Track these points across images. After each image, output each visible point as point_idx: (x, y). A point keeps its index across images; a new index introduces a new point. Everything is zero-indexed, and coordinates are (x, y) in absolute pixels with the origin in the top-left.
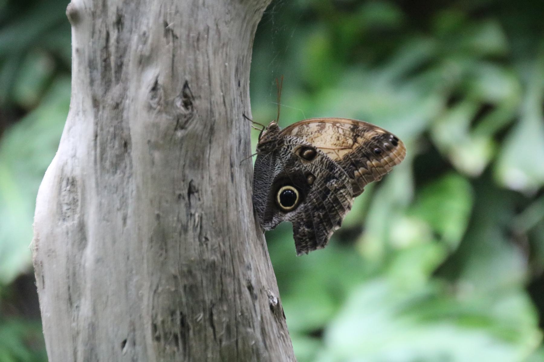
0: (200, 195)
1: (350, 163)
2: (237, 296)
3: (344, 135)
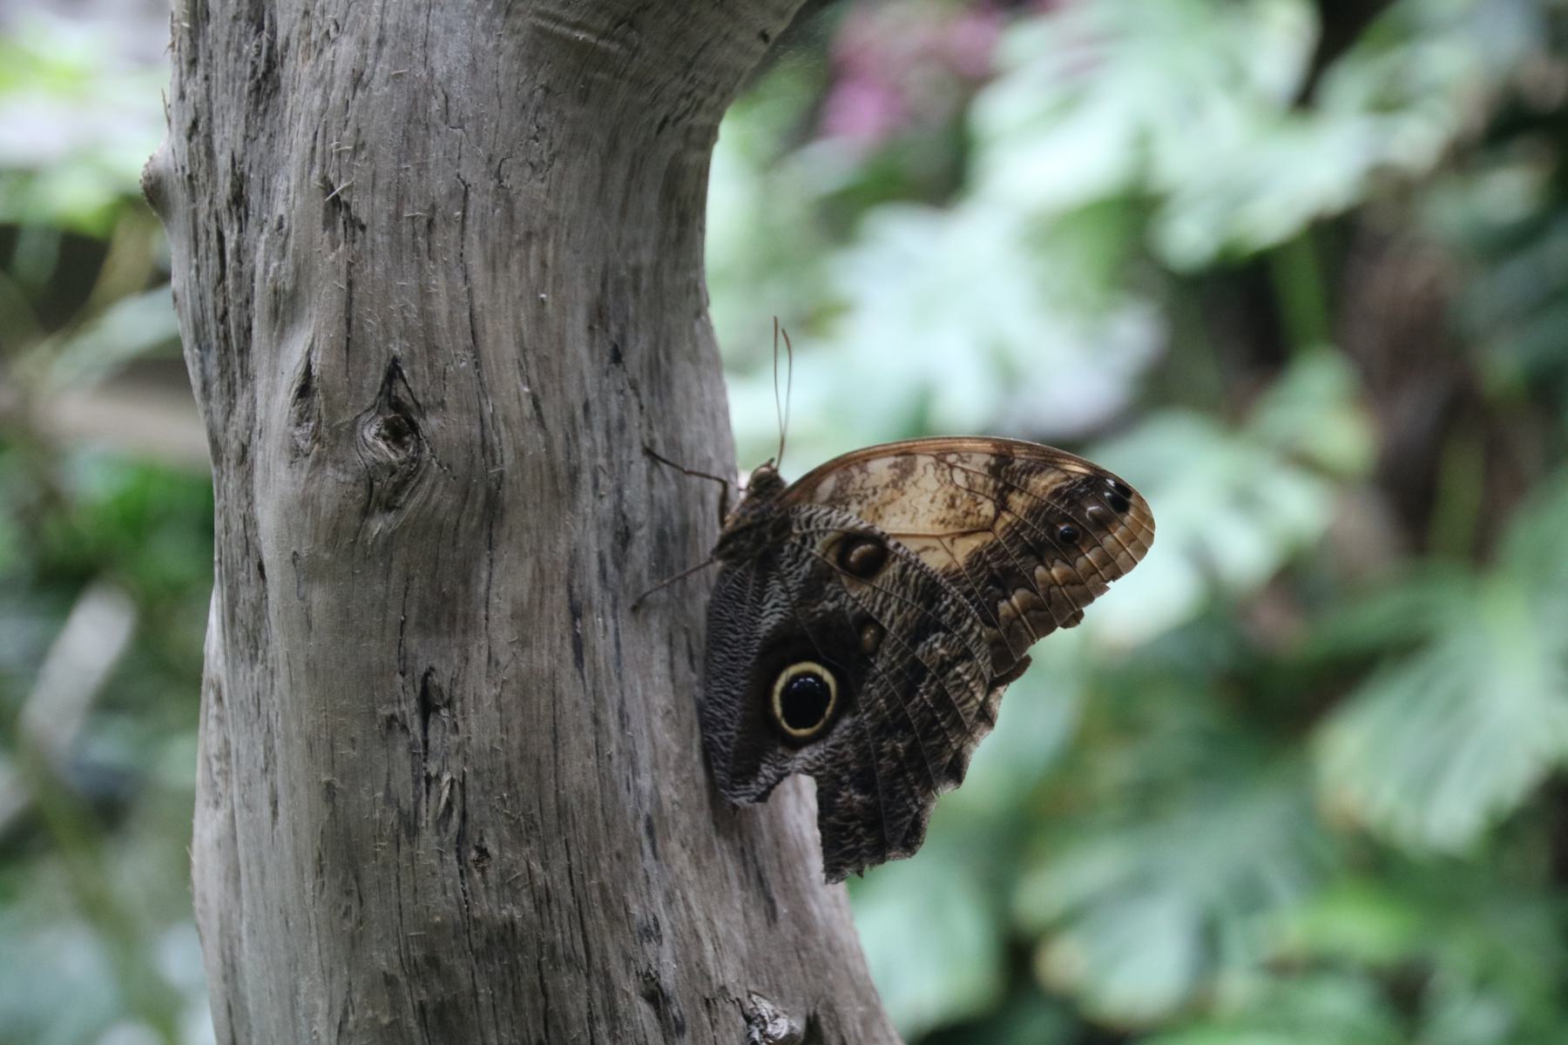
0: (458, 712)
1: (986, 578)
2: (602, 1028)
3: (969, 490)
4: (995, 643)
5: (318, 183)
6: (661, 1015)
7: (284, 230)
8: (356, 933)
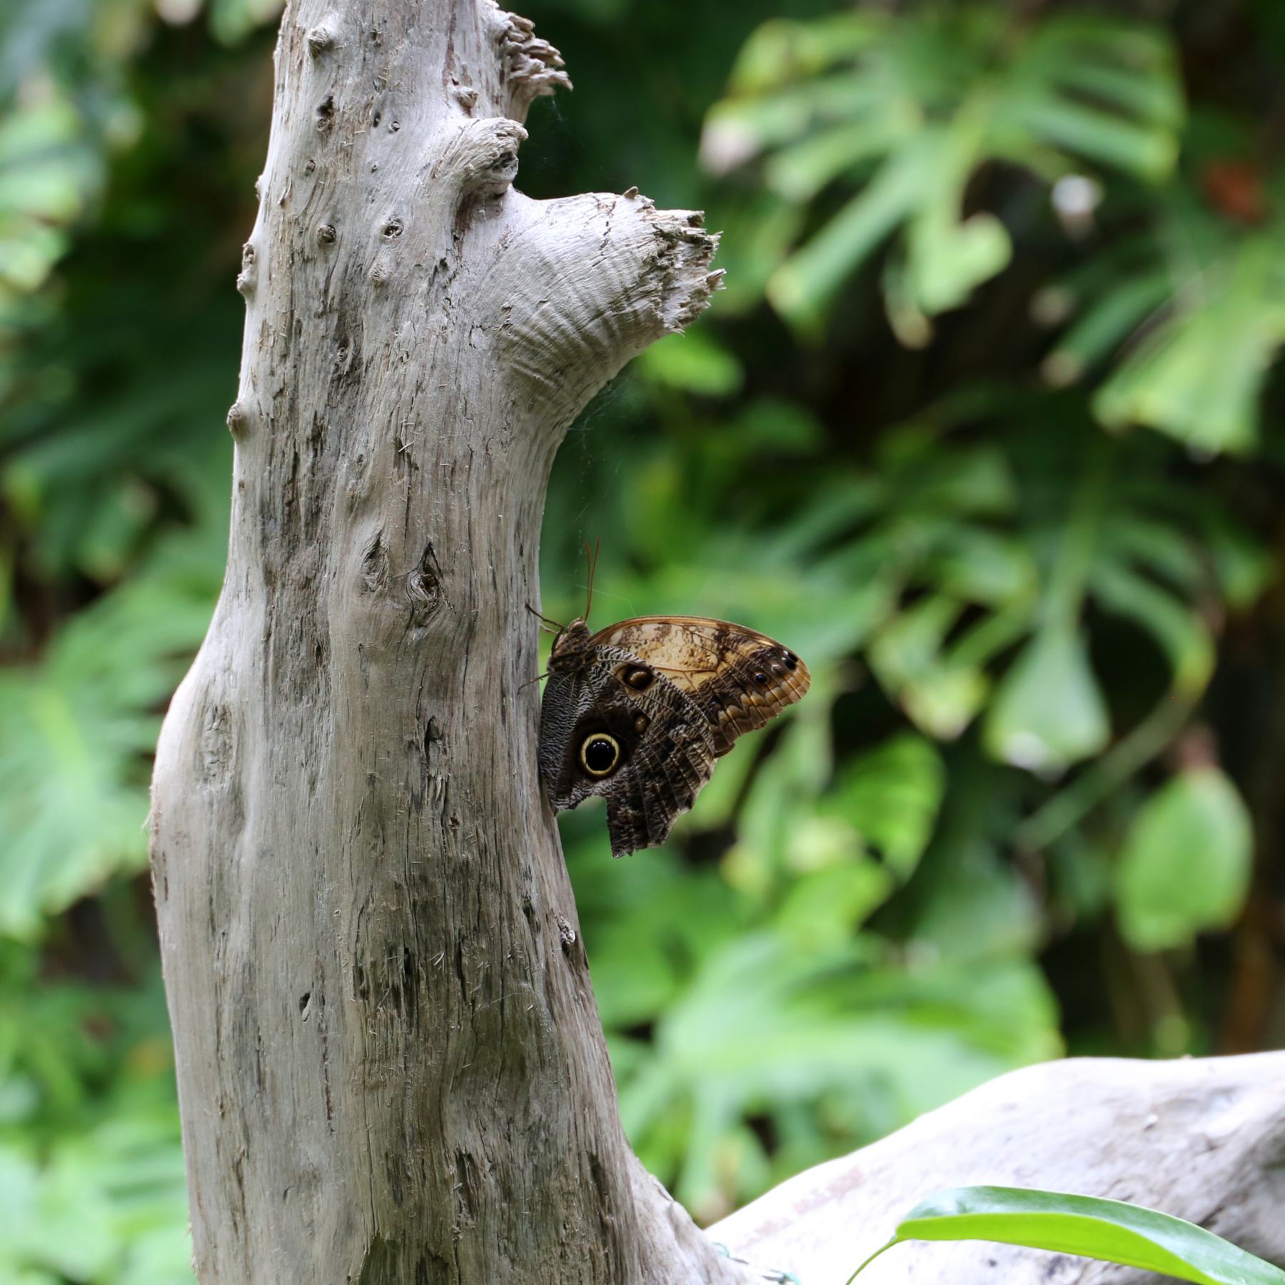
2: (506, 924)
3: (702, 647)
4: (715, 734)
6: (530, 921)
7: (363, 463)
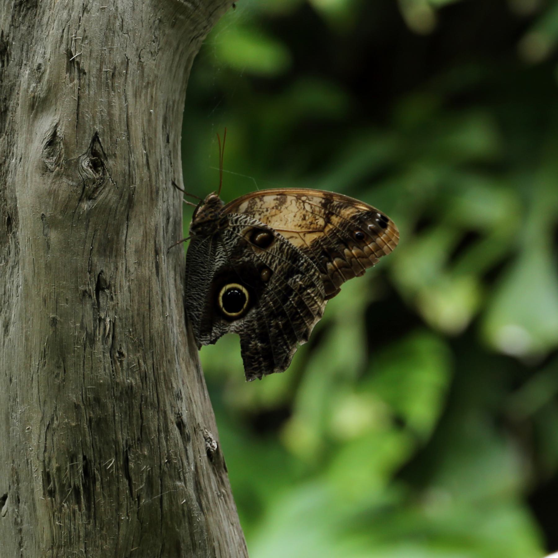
0: (113, 291)
1: (321, 252)
2: (163, 435)
3: (312, 213)
4: (325, 281)
5: (64, 52)
6: (182, 432)
7: (41, 70)
8: (62, 385)
